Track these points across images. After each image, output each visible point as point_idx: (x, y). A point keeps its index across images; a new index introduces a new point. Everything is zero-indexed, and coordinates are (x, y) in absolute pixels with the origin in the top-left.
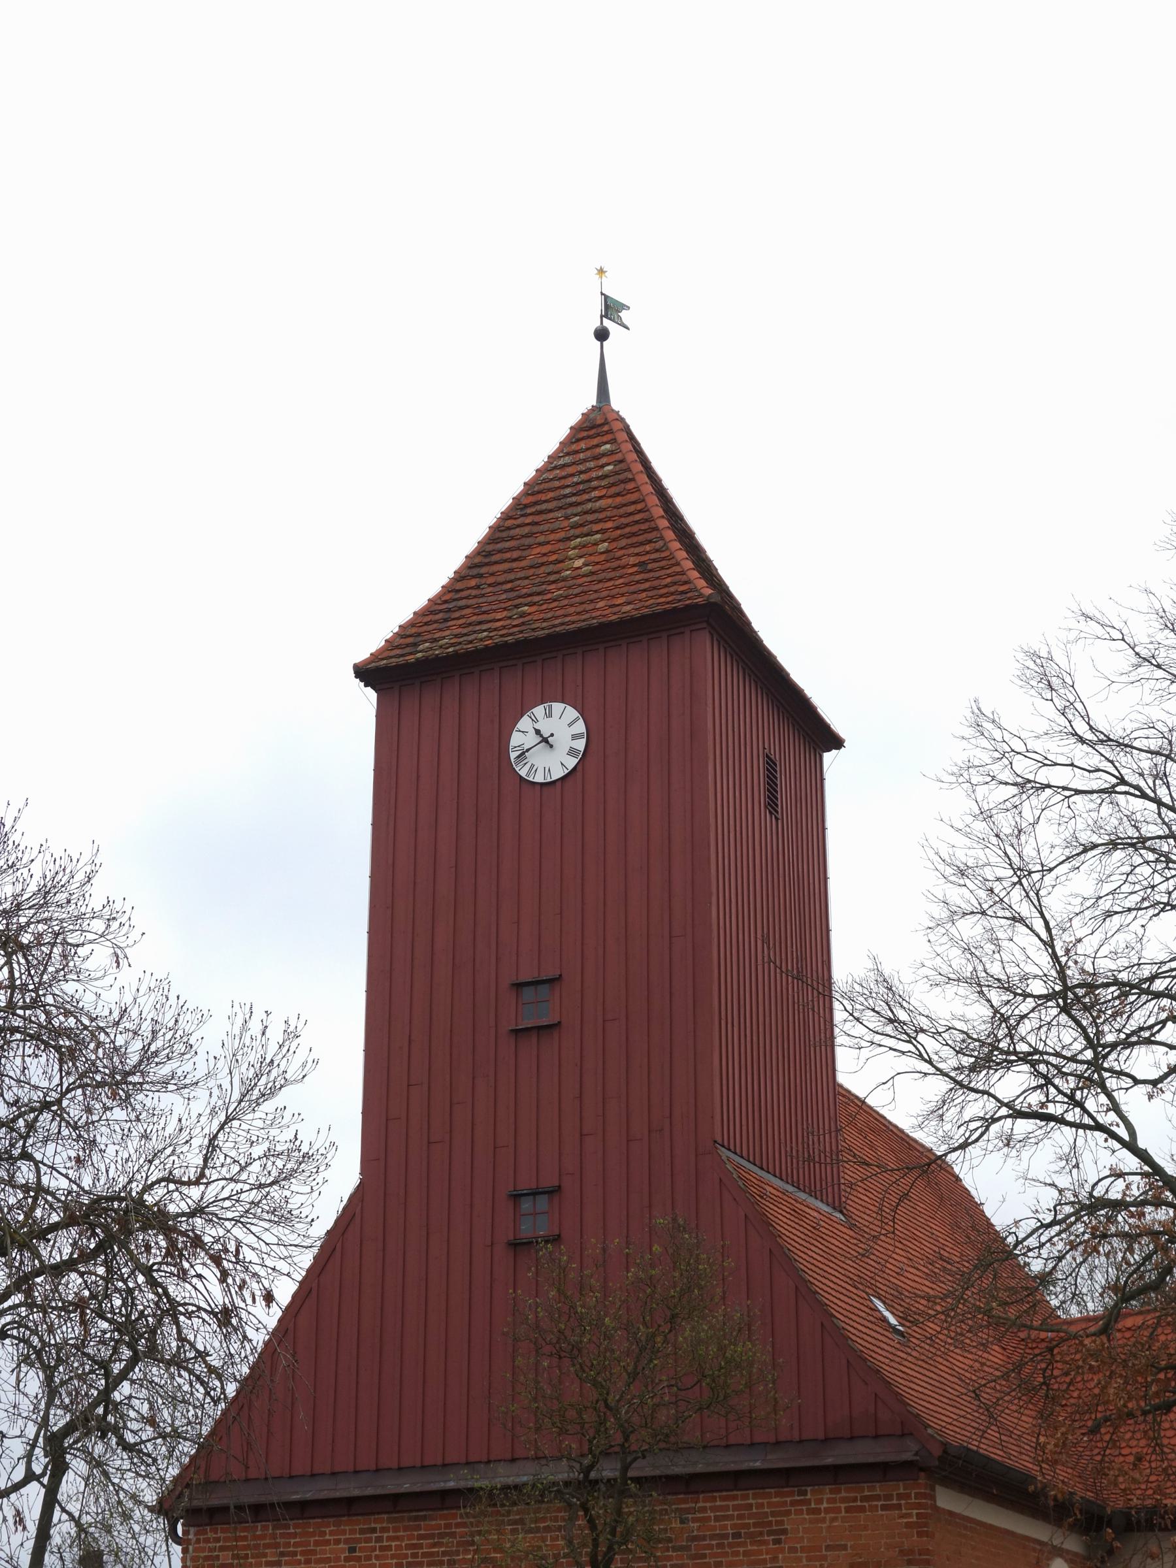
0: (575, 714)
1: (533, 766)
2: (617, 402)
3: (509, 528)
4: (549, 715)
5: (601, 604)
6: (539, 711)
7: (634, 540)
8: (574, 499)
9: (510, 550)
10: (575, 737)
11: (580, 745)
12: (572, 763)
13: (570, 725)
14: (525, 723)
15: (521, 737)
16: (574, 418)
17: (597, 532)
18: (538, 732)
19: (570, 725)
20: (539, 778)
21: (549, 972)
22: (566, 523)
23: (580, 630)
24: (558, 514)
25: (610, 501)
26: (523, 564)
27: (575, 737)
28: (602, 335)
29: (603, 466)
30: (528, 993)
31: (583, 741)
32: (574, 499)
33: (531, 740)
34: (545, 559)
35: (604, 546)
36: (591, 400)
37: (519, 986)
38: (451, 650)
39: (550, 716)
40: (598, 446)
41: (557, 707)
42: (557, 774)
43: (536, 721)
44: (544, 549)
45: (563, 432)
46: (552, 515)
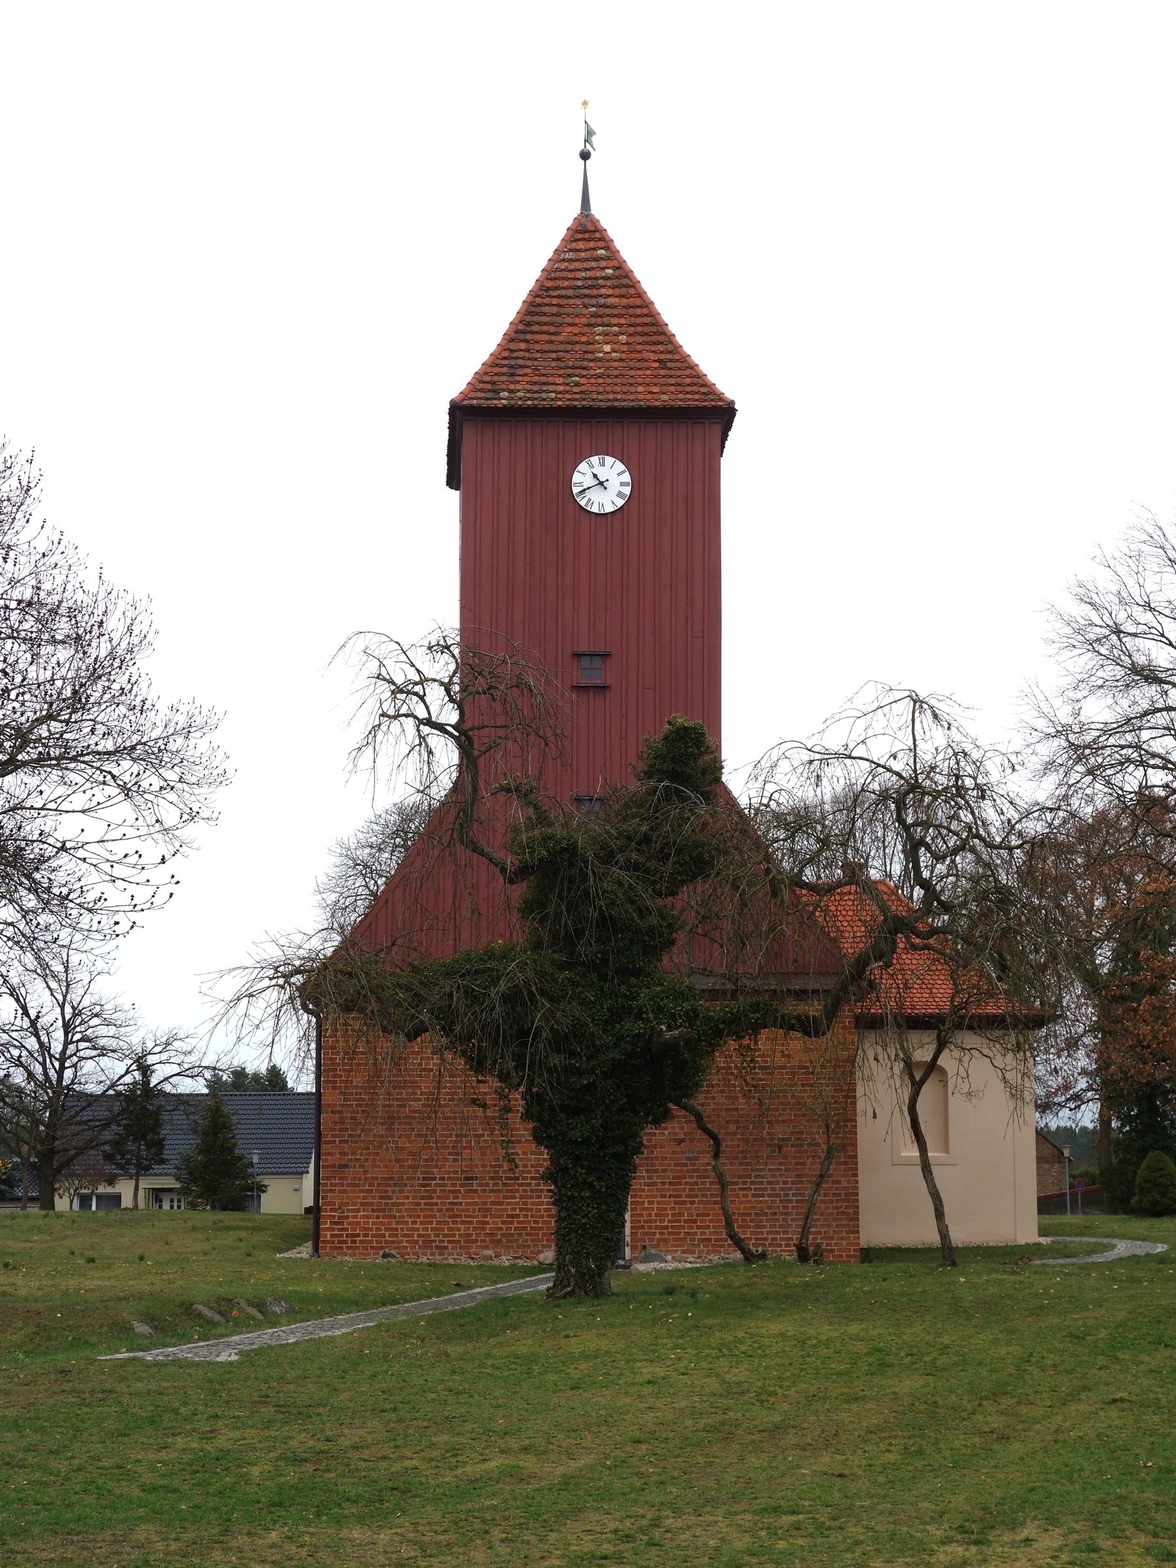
0: (623, 467)
1: (590, 499)
2: (596, 211)
3: (539, 305)
4: (603, 464)
5: (640, 389)
6: (595, 460)
7: (648, 339)
8: (587, 292)
9: (545, 324)
10: (622, 484)
11: (627, 491)
12: (620, 503)
13: (619, 474)
14: (583, 466)
15: (582, 476)
16: (569, 222)
17: (615, 325)
18: (595, 476)
19: (619, 474)
20: (595, 509)
21: (601, 649)
22: (585, 311)
23: (633, 408)
24: (578, 301)
25: (617, 300)
26: (560, 338)
27: (622, 484)
28: (585, 156)
29: (603, 269)
30: (585, 662)
31: (629, 488)
32: (587, 292)
33: (589, 481)
34: (577, 339)
35: (623, 338)
36: (576, 210)
37: (578, 656)
38: (530, 403)
39: (603, 465)
40: (594, 249)
41: (609, 460)
42: (609, 509)
43: (592, 467)
44: (576, 330)
45: (562, 233)
46: (571, 301)
